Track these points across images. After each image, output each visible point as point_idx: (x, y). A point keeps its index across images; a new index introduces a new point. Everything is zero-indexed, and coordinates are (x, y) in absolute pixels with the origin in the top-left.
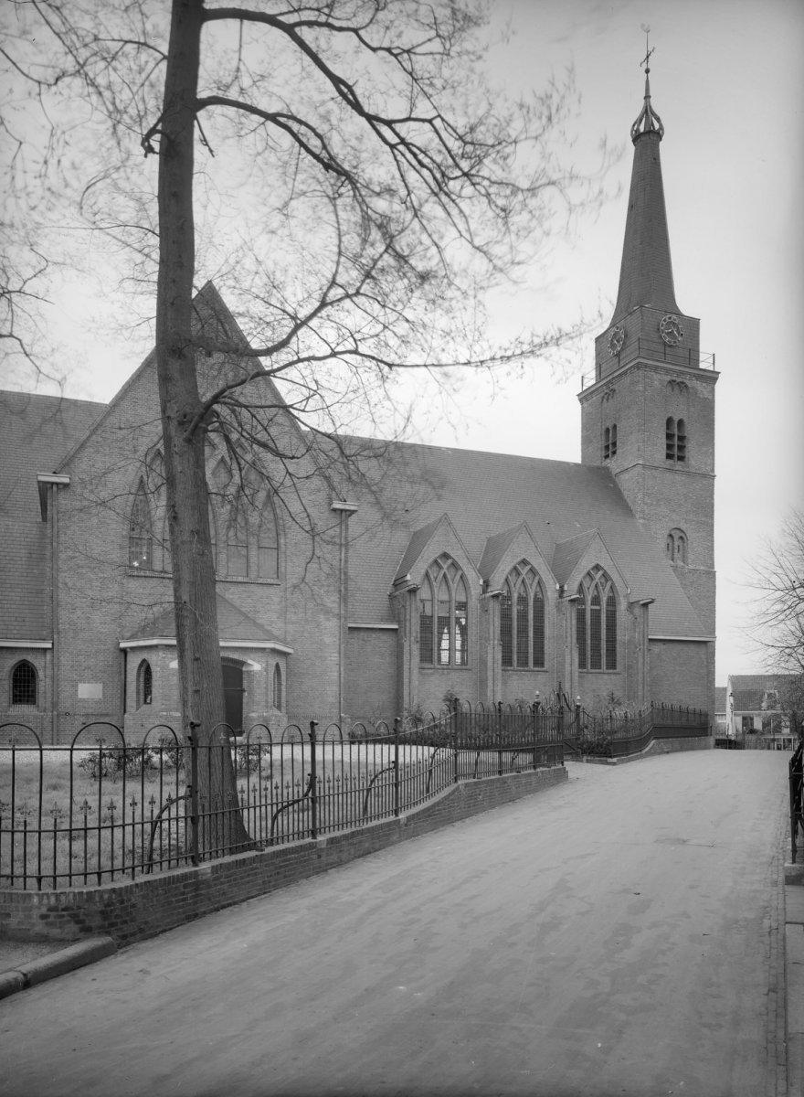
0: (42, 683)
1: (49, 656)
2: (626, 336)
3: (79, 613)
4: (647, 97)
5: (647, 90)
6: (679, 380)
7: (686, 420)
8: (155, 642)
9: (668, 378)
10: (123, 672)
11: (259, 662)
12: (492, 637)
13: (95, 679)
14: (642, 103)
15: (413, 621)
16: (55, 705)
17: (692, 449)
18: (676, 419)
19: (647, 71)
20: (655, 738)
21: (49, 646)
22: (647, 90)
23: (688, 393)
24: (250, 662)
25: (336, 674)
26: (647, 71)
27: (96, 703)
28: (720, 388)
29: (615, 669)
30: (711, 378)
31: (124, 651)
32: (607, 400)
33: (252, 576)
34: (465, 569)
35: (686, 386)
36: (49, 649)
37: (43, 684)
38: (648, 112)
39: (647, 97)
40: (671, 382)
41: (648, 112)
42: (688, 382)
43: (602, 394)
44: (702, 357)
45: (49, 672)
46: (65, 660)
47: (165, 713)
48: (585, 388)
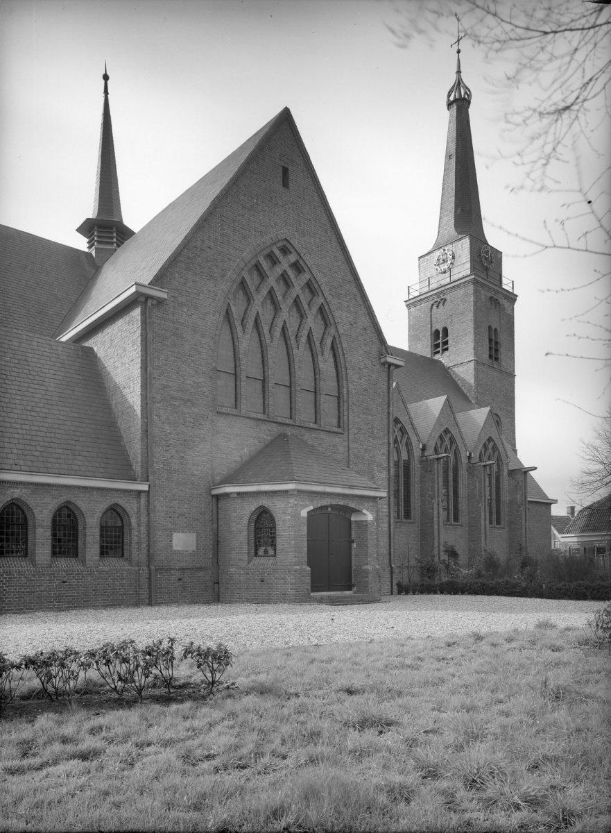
0: (135, 533)
1: (143, 500)
2: (454, 258)
3: (173, 451)
4: (459, 72)
5: (459, 66)
6: (495, 297)
7: (499, 329)
8: (290, 486)
9: (489, 295)
10: (215, 520)
11: (370, 511)
12: (436, 495)
13: (188, 528)
14: (454, 78)
15: (417, 476)
16: (150, 558)
17: (502, 350)
18: (493, 328)
19: (459, 52)
20: (312, 571)
21: (145, 488)
22: (459, 66)
23: (500, 307)
24: (364, 511)
25: (386, 525)
26: (459, 52)
27: (191, 555)
28: (518, 306)
29: (458, 522)
30: (512, 298)
31: (218, 498)
32: (438, 307)
33: (323, 426)
34: (410, 433)
35: (499, 303)
36: (144, 491)
37: (136, 535)
38: (459, 83)
39: (459, 72)
40: (491, 298)
41: (459, 83)
42: (499, 299)
43: (432, 302)
44: (504, 281)
45: (144, 519)
46: (159, 504)
47: (298, 567)
48: (411, 297)
